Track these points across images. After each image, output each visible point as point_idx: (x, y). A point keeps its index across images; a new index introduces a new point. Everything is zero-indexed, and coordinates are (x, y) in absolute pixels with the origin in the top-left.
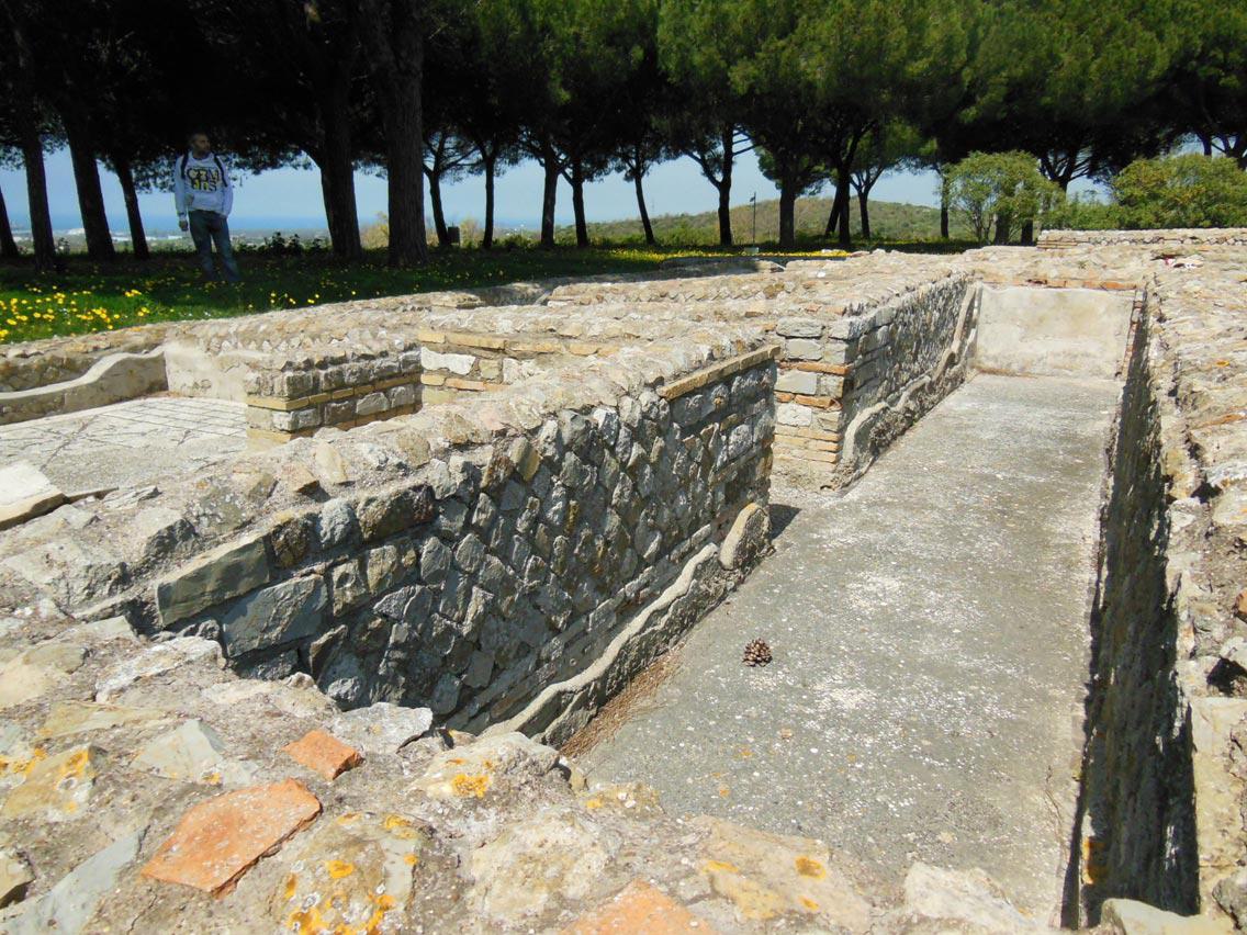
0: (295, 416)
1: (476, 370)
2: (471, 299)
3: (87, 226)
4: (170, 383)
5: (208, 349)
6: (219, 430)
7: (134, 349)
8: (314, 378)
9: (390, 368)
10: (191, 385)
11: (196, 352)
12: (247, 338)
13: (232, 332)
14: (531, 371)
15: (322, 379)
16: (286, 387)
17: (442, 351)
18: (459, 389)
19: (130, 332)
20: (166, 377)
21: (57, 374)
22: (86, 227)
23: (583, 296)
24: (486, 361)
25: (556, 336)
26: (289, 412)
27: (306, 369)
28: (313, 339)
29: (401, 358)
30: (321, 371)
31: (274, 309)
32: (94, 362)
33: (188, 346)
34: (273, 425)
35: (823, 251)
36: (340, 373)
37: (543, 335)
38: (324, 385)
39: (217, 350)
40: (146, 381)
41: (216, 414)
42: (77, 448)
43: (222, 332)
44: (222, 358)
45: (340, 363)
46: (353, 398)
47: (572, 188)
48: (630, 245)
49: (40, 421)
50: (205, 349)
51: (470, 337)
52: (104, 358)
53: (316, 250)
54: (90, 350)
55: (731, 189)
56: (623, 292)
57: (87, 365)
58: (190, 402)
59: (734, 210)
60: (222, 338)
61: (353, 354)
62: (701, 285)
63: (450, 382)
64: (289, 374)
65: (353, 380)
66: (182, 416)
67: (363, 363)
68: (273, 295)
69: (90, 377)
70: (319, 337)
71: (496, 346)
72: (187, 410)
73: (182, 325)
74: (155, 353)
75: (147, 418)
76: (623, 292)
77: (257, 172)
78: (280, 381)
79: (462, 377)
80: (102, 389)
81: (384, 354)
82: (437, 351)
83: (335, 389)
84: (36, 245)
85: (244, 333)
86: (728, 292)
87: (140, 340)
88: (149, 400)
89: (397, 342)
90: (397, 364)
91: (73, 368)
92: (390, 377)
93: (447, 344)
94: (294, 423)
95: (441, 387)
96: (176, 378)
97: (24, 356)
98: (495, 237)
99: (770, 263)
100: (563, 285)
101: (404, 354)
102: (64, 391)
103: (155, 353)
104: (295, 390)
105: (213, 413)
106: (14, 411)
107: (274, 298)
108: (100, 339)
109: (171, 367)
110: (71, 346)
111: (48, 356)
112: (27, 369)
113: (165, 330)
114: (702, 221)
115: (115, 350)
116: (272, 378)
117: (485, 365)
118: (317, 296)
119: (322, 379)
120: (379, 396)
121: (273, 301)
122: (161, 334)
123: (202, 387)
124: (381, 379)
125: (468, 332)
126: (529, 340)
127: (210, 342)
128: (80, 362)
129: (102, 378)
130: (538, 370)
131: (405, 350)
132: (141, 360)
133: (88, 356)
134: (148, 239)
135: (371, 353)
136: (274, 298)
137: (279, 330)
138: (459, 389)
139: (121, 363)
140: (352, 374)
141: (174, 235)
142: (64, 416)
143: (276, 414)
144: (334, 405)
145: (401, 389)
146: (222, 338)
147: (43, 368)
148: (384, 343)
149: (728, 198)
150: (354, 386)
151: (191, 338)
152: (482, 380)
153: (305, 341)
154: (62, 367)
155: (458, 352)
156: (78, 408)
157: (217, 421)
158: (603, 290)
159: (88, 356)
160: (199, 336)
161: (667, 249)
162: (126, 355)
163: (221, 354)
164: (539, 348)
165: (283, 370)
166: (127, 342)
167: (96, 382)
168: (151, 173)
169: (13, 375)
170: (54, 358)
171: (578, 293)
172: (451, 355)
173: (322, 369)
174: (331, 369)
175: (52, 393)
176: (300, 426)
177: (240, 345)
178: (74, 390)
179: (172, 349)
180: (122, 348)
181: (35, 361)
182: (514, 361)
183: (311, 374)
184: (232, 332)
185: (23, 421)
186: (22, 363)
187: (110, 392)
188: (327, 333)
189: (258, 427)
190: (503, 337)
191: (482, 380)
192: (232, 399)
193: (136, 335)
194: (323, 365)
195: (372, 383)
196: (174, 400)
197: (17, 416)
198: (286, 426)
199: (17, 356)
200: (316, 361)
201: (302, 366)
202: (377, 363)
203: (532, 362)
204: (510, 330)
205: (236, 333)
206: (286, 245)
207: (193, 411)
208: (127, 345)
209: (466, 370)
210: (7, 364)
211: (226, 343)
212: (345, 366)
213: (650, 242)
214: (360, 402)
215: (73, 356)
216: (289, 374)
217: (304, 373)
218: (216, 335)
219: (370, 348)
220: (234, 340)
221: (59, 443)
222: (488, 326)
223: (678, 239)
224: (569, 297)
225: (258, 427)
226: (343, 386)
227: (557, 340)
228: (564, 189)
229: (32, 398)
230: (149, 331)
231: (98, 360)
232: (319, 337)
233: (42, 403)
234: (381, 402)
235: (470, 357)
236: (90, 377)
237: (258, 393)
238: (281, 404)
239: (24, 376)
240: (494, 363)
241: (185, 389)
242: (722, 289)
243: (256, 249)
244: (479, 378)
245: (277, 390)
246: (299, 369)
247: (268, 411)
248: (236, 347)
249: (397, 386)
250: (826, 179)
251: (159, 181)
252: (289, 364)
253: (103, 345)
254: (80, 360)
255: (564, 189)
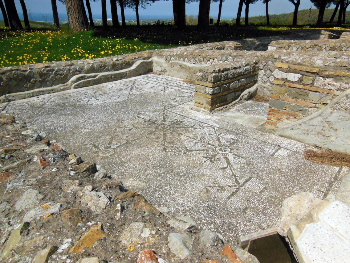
0: (214, 90)
1: (301, 80)
2: (238, 44)
3: (113, 18)
4: (153, 69)
5: (166, 60)
6: (174, 88)
7: (145, 59)
8: (220, 76)
9: (241, 72)
10: (160, 71)
11: (162, 60)
12: (180, 56)
13: (175, 54)
14: (330, 83)
15: (223, 76)
16: (213, 79)
17: (285, 71)
18: (290, 87)
19: (143, 53)
20: (152, 68)
21: (125, 66)
22: (122, 21)
23: (282, 45)
24: (307, 77)
25: (347, 69)
26: (212, 88)
27: (218, 73)
28: (204, 59)
29: (244, 69)
30: (223, 73)
31: (180, 46)
32: (135, 62)
33: (160, 58)
34: (205, 92)
35: (335, 28)
36: (228, 74)
37: (340, 68)
38: (223, 79)
39: (169, 60)
40: (146, 69)
41: (170, 81)
42: (135, 91)
43: (171, 54)
44: (171, 63)
45: (228, 70)
46: (230, 83)
47: (295, 6)
48: (262, 25)
49: (121, 81)
50: (165, 59)
51: (300, 67)
52: (137, 61)
53: (169, 26)
54: (134, 58)
55: (299, 6)
56: (299, 44)
57: (133, 63)
58: (161, 77)
59: (299, 11)
60: (171, 56)
61: (232, 67)
62: (333, 42)
63: (287, 84)
64: (214, 74)
65: (231, 76)
66: (160, 82)
67: (234, 71)
68: (180, 41)
69: (133, 67)
70: (206, 58)
71: (314, 71)
72: (161, 78)
73: (157, 51)
74: (150, 60)
75: (151, 82)
76: (299, 44)
77: (154, 2)
78: (211, 77)
79: (293, 82)
80: (136, 71)
81: (240, 67)
82: (283, 71)
83: (226, 80)
84: (123, 24)
85: (179, 54)
86: (345, 45)
87: (146, 56)
88: (148, 75)
89: (243, 63)
90: (243, 71)
91: (129, 64)
92: (240, 76)
93: (289, 69)
94: (213, 92)
95: (281, 85)
96: (156, 68)
97: (117, 60)
98: (220, 22)
99: (328, 32)
100: (274, 40)
101: (245, 68)
102: (127, 72)
103: (150, 60)
104: (215, 80)
105: (169, 81)
106: (115, 77)
107: (180, 42)
108: (136, 55)
109: (154, 64)
110: (129, 57)
111: (123, 60)
112: (118, 64)
113: (153, 53)
114: (281, 16)
115: (140, 59)
116: (208, 75)
117: (306, 78)
118: (192, 42)
119: (223, 76)
120: (236, 82)
121: (179, 43)
122: (151, 53)
123: (163, 72)
124: (238, 76)
125: (300, 64)
126: (331, 69)
127: (167, 57)
128: (131, 62)
129: (136, 68)
130: (334, 83)
131: (245, 66)
132: (146, 62)
133: (133, 61)
134: (126, 21)
135: (236, 67)
136: (180, 42)
137: (191, 55)
138: (290, 87)
139: (142, 63)
140: (231, 74)
141: (127, 20)
142: (127, 79)
143: (207, 88)
144: (224, 85)
145: (243, 80)
146: (171, 56)
147: (122, 64)
148: (240, 63)
149: (90, 9)
150: (230, 79)
151: (161, 56)
152: (303, 84)
153: (201, 59)
154: (127, 64)
155: (293, 73)
156: (130, 77)
157: (172, 84)
158: (291, 43)
159: (133, 61)
160: (163, 55)
161: (276, 26)
162: (142, 61)
163: (171, 62)
164: (337, 74)
165: (212, 73)
166: (143, 56)
167: (135, 69)
168: (126, 3)
169: (115, 66)
170: (125, 61)
171: (280, 44)
172: (290, 74)
173: (223, 73)
174: (225, 73)
175: (124, 72)
176: (215, 93)
177: (177, 59)
178: (129, 71)
179: (155, 59)
180: (141, 58)
181: (120, 62)
182: (321, 78)
183: (219, 74)
184: (175, 54)
185: (117, 80)
186: (117, 62)
187: (138, 72)
188: (209, 57)
189: (200, 92)
190: (318, 68)
191: (303, 84)
192: (173, 76)
193: (145, 54)
194: (223, 71)
195: (235, 78)
196: (156, 75)
197: (115, 79)
198: (211, 93)
199: (116, 60)
200: (222, 70)
201: (218, 71)
202: (238, 70)
203: (331, 79)
204: (322, 65)
205: (176, 55)
206: (161, 24)
207: (163, 80)
208: (143, 57)
209: (297, 79)
210: (114, 62)
211: (172, 58)
212: (229, 71)
213: (268, 24)
214: (231, 84)
215: (129, 60)
216: (214, 74)
217: (218, 74)
218: (169, 55)
219: (236, 65)
220: (175, 57)
221: (129, 89)
222: (311, 62)
223: (275, 23)
224: (277, 45)
225: (200, 92)
226: (228, 78)
227: (347, 71)
228: (244, 6)
229: (119, 73)
230: (148, 53)
231: (136, 62)
232: (206, 58)
233: (122, 75)
234: (237, 85)
235: (299, 74)
236: (133, 67)
237: (201, 80)
238: (210, 85)
239: (117, 66)
240: (311, 78)
241: (158, 72)
242: (342, 44)
243: (152, 25)
244: (301, 83)
245: (209, 79)
246: (216, 72)
247: (204, 87)
248: (176, 59)
249: (242, 79)
250: (332, 2)
251: (128, 5)
252: (214, 71)
253: (137, 57)
254: (131, 61)
255: (244, 6)
